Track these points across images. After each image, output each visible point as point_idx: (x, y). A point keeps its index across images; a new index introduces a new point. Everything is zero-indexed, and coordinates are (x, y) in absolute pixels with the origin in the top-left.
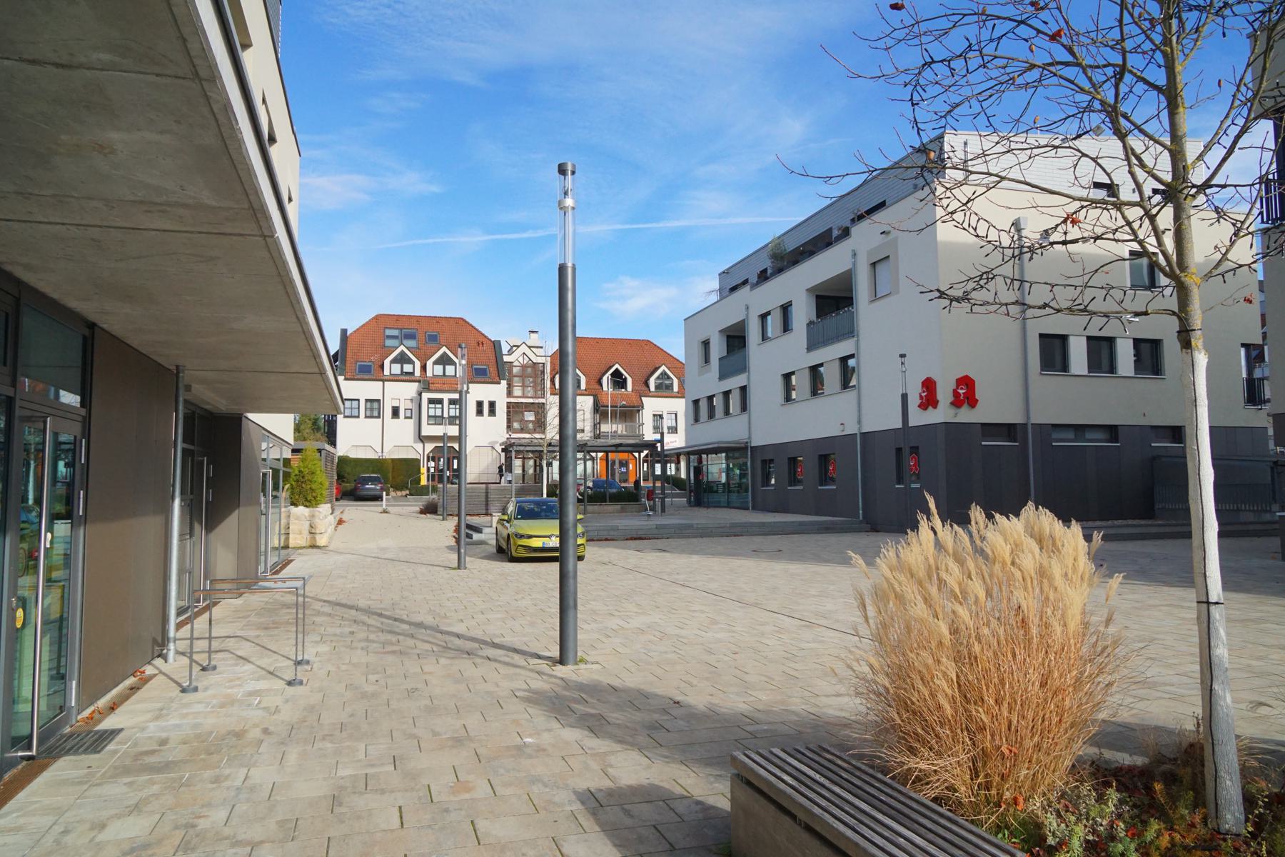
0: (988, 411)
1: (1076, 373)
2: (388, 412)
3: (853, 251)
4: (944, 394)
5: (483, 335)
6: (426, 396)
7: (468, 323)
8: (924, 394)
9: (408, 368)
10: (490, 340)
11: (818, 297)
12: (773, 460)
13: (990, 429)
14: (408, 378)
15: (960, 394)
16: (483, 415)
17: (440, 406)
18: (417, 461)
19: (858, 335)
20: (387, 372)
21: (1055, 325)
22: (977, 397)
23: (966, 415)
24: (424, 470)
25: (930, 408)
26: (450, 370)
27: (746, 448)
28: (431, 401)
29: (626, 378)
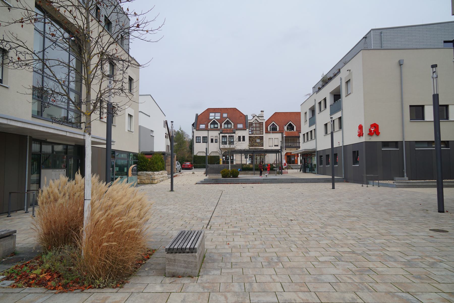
0: (384, 137)
1: (427, 120)
2: (210, 141)
3: (341, 78)
4: (365, 131)
5: (242, 113)
6: (221, 135)
7: (237, 110)
8: (359, 131)
9: (216, 126)
10: (244, 115)
11: (335, 95)
12: (322, 156)
13: (386, 144)
14: (216, 129)
15: (372, 131)
16: (213, 142)
17: (226, 138)
18: (218, 156)
19: (342, 109)
20: (209, 127)
21: (212, 138)
22: (379, 131)
23: (374, 139)
24: (221, 160)
25: (361, 137)
26: (229, 126)
27: (315, 152)
28: (223, 136)
29: (294, 126)
